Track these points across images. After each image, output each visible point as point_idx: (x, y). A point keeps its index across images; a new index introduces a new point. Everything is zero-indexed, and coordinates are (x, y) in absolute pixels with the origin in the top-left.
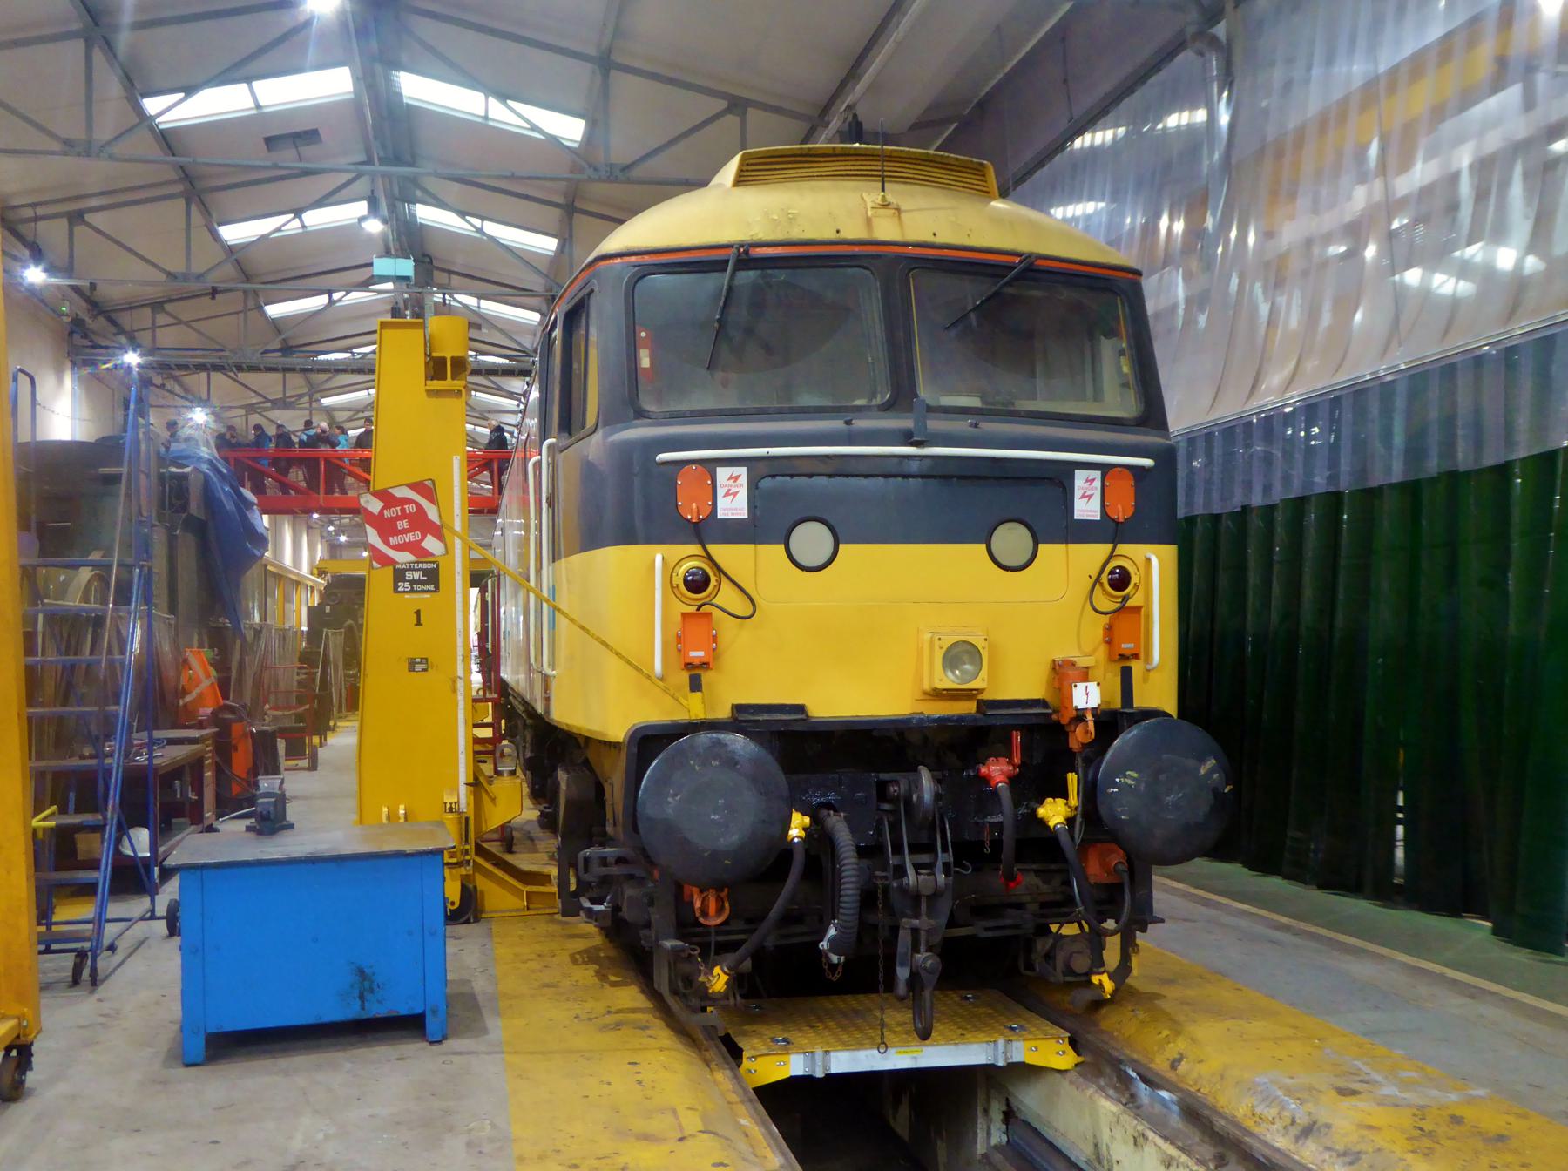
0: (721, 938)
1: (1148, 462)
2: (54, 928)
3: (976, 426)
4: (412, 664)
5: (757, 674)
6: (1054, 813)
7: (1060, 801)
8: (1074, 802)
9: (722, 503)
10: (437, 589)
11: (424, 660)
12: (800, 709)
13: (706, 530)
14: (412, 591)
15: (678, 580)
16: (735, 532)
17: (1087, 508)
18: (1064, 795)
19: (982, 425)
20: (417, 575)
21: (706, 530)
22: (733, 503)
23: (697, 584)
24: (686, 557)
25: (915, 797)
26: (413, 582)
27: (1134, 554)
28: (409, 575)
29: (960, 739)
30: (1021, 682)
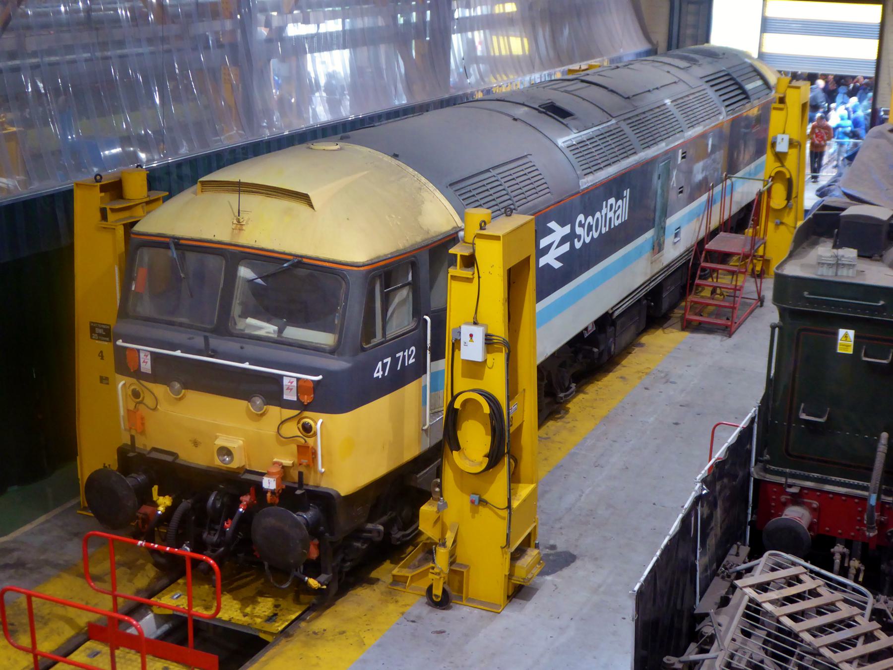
9: (142, 365)
13: (138, 374)
20: (101, 331)
26: (99, 335)
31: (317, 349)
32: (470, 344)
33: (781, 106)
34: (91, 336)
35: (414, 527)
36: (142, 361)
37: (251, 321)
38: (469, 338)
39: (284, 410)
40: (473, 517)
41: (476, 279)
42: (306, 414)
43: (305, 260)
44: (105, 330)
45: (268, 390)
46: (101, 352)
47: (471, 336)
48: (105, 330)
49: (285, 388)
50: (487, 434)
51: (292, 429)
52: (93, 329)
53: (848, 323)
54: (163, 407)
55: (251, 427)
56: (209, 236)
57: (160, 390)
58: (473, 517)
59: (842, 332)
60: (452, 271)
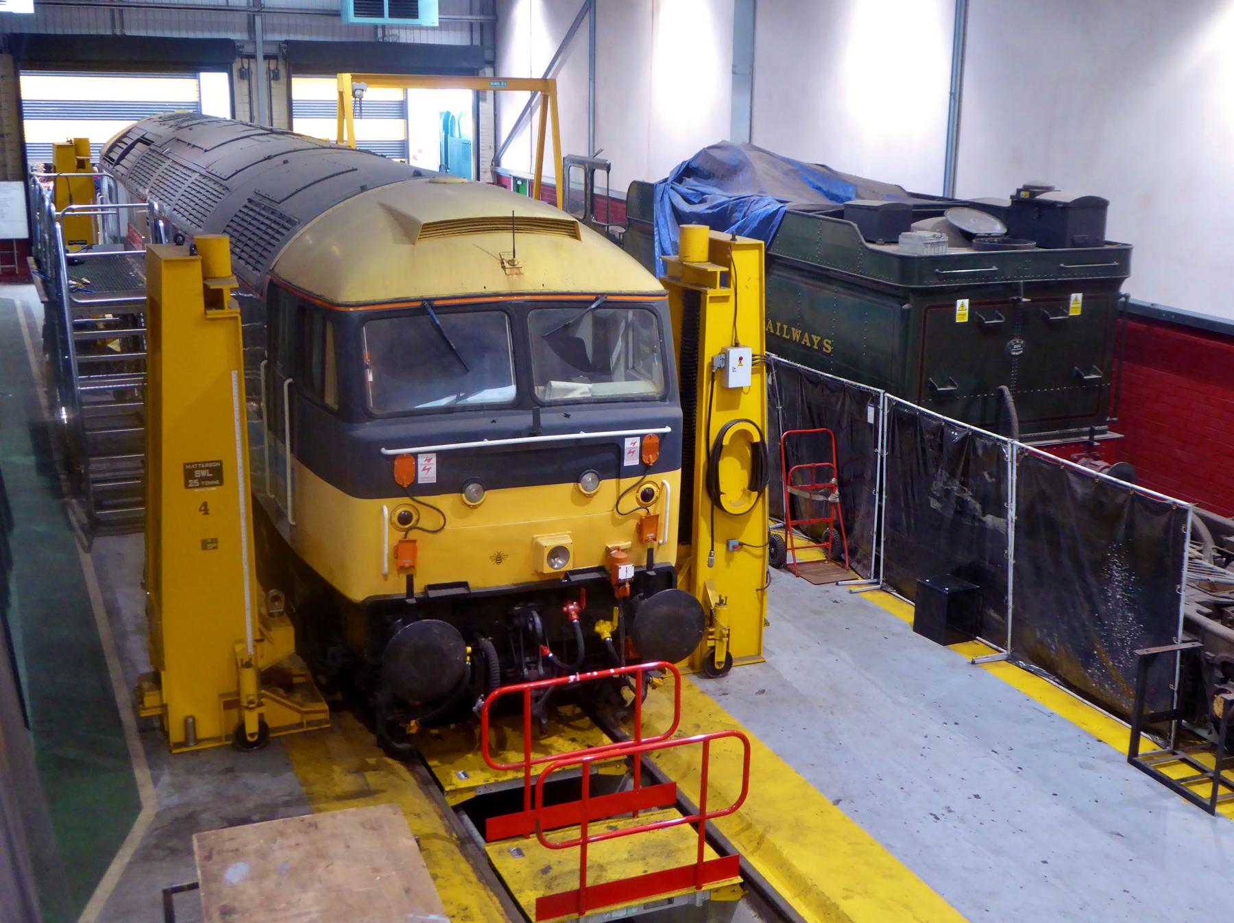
0: (99, 219)
1: (668, 429)
2: (1087, 429)
3: (567, 416)
4: (205, 545)
5: (435, 569)
6: (605, 630)
7: (608, 623)
8: (616, 624)
9: (421, 474)
10: (221, 483)
11: (215, 541)
12: (464, 585)
13: (416, 490)
14: (201, 486)
15: (395, 519)
16: (429, 490)
17: (631, 461)
18: (611, 620)
19: (572, 414)
20: (204, 473)
21: (416, 490)
22: (428, 471)
23: (405, 519)
24: (402, 504)
25: (530, 626)
26: (201, 479)
27: (653, 481)
28: (198, 474)
29: (548, 593)
30: (584, 559)
31: (645, 400)
32: (738, 369)
33: (487, 177)
34: (187, 486)
35: (877, 550)
36: (420, 468)
37: (555, 384)
38: (737, 361)
39: (623, 481)
40: (728, 566)
41: (732, 298)
42: (649, 477)
43: (609, 298)
44: (211, 470)
45: (604, 459)
46: (205, 504)
47: (741, 359)
48: (211, 470)
49: (626, 452)
50: (743, 468)
51: (631, 502)
52: (189, 474)
53: (962, 292)
54: (453, 524)
55: (580, 514)
56: (478, 289)
57: (445, 502)
58: (728, 566)
59: (959, 302)
60: (711, 293)
